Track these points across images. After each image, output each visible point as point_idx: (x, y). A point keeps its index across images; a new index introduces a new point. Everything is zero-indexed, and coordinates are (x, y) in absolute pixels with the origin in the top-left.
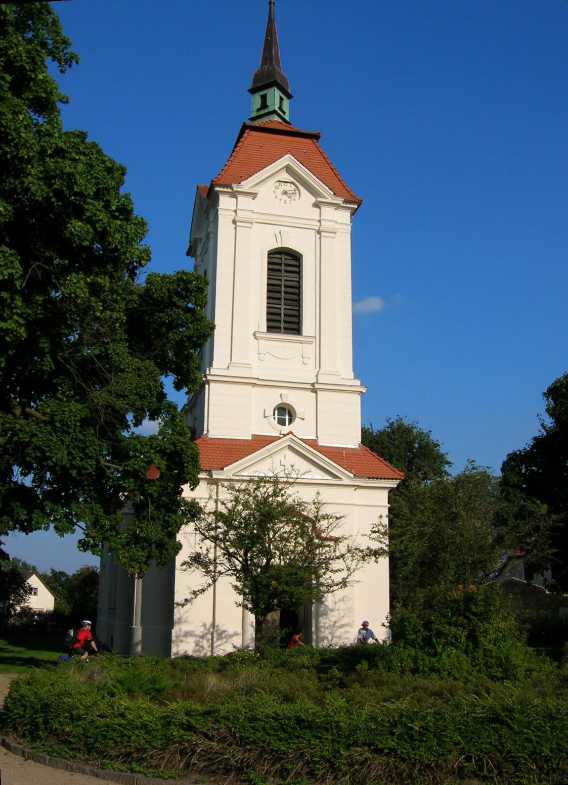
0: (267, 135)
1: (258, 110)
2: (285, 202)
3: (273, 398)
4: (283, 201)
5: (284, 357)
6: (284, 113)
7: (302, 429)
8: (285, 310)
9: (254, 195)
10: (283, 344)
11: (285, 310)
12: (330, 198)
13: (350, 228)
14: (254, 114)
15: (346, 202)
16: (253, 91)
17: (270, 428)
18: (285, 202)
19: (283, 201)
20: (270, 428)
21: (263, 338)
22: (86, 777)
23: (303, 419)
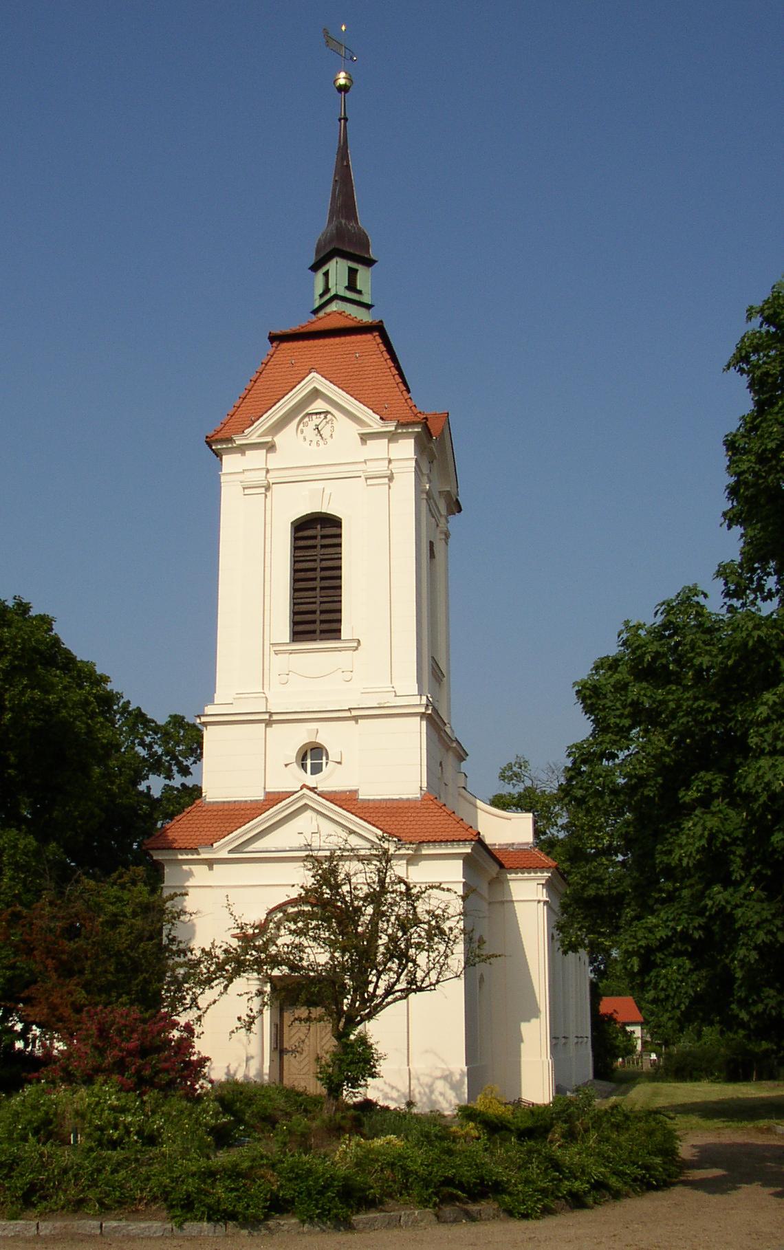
0: (306, 343)
1: (321, 296)
2: (318, 444)
3: (301, 735)
4: (314, 443)
5: (317, 676)
6: (360, 292)
7: (331, 779)
8: (316, 608)
9: (271, 447)
10: (317, 657)
11: (316, 608)
12: (375, 426)
13: (413, 463)
14: (317, 305)
15: (401, 425)
16: (315, 268)
17: (291, 778)
18: (318, 444)
19: (314, 443)
20: (291, 778)
21: (284, 652)
22: (627, 1202)
23: (340, 763)
